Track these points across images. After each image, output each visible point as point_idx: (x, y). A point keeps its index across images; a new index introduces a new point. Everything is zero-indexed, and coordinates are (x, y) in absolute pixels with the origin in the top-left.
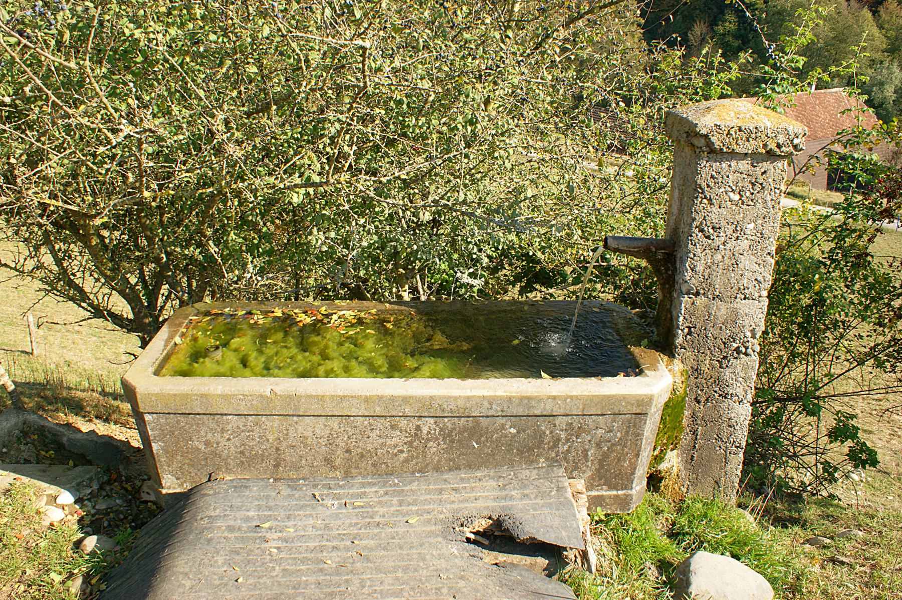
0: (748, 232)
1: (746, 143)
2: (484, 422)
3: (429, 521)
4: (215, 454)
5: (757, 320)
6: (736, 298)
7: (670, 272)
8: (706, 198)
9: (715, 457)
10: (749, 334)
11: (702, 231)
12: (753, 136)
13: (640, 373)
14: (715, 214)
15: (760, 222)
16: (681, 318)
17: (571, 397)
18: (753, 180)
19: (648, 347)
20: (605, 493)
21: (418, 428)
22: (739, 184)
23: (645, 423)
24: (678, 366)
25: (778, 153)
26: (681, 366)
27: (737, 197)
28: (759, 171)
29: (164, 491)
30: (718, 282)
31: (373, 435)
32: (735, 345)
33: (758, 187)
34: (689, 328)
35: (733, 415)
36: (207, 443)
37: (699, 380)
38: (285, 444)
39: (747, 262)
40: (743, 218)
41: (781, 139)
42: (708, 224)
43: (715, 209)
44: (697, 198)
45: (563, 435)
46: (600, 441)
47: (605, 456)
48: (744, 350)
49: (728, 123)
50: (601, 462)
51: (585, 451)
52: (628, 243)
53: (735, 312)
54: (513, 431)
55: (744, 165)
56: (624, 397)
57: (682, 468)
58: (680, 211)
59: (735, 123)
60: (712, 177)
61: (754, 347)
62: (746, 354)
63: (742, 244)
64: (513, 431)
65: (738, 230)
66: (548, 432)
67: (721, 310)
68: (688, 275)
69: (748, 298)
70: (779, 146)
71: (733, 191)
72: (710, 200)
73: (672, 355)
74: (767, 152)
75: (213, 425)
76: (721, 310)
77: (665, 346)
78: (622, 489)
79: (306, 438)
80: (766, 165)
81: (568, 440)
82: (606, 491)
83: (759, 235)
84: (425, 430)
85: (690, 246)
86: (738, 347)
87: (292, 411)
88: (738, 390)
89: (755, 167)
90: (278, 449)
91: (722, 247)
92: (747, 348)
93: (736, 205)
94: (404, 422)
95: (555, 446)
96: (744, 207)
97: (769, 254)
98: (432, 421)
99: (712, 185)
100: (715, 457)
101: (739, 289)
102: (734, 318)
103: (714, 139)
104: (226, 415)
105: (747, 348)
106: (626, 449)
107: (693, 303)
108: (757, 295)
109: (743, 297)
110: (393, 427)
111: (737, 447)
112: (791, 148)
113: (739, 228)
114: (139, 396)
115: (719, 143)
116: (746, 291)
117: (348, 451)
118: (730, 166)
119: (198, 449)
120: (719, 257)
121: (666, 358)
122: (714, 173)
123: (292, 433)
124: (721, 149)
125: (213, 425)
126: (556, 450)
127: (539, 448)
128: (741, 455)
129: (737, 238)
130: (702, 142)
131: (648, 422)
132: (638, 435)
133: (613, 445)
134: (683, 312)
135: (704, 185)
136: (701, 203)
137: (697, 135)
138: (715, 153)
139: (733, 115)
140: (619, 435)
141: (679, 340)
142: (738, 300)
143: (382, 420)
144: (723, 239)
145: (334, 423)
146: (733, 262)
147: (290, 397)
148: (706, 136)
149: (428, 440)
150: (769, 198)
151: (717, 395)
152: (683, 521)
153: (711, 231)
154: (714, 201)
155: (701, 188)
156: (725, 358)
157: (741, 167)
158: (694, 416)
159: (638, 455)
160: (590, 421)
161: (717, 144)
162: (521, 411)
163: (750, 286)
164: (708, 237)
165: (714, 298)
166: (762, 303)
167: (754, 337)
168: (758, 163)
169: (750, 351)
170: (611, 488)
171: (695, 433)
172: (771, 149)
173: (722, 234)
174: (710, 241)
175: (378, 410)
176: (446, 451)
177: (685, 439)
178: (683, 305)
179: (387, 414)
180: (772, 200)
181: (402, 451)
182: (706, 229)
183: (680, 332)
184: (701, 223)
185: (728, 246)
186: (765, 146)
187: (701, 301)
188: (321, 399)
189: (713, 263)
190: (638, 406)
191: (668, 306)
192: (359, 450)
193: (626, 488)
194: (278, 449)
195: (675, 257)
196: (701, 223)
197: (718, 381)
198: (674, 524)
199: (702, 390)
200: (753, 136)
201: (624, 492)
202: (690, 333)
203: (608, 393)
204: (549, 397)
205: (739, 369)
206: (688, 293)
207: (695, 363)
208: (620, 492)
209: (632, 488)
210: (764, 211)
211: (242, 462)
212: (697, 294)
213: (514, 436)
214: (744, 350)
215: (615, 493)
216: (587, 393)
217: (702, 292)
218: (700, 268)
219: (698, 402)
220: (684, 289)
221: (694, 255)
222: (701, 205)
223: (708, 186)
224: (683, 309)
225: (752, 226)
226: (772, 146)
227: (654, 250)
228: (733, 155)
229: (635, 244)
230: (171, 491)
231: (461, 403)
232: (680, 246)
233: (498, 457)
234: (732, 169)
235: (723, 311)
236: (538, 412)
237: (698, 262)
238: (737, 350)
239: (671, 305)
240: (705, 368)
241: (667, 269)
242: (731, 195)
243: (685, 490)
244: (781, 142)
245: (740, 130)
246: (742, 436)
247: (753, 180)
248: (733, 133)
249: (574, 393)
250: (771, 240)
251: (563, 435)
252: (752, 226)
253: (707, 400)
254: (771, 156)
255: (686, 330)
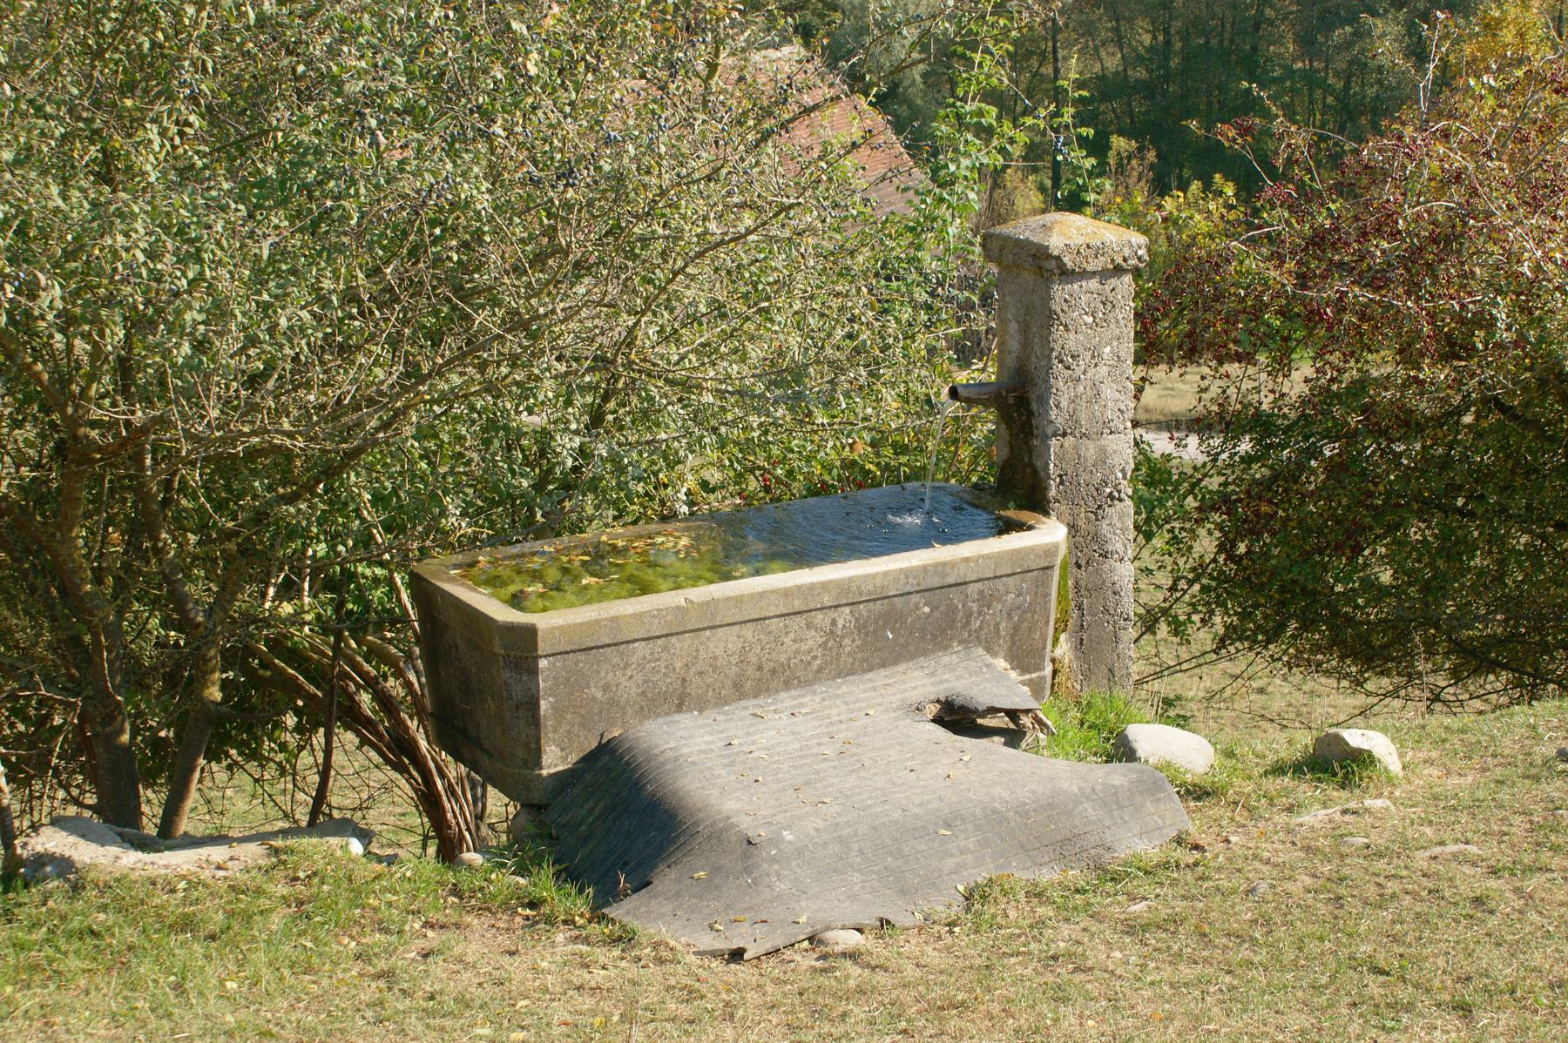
2: (898, 602)
3: (886, 710)
4: (612, 702)
10: (1120, 475)
11: (1061, 361)
14: (1072, 341)
21: (834, 623)
27: (1090, 320)
28: (1108, 288)
29: (544, 772)
30: (1083, 417)
31: (788, 641)
33: (1109, 306)
36: (606, 688)
38: (692, 672)
39: (1108, 391)
43: (1072, 336)
47: (1016, 628)
50: (1013, 636)
51: (997, 625)
52: (977, 389)
53: (1103, 450)
54: (927, 609)
55: (1093, 284)
58: (1026, 343)
59: (1080, 240)
62: (1120, 500)
64: (927, 609)
65: (1096, 355)
67: (1090, 450)
68: (1053, 413)
70: (1125, 260)
75: (616, 660)
76: (1090, 450)
79: (716, 658)
80: (1113, 282)
81: (980, 613)
84: (840, 623)
87: (709, 622)
90: (684, 680)
94: (820, 616)
95: (968, 623)
98: (847, 610)
102: (1103, 454)
103: (1066, 260)
104: (628, 642)
110: (809, 626)
114: (540, 639)
117: (760, 668)
119: (594, 699)
120: (1081, 388)
123: (702, 655)
125: (616, 660)
130: (1053, 264)
132: (1047, 595)
137: (1049, 257)
138: (1067, 275)
141: (1052, 493)
143: (798, 618)
145: (748, 631)
147: (707, 603)
148: (1058, 258)
149: (843, 637)
158: (1077, 586)
160: (999, 584)
161: (1070, 265)
162: (936, 582)
164: (1068, 368)
167: (1124, 478)
175: (798, 605)
176: (860, 649)
179: (800, 609)
181: (815, 658)
185: (1089, 375)
186: (1113, 261)
187: (1069, 441)
188: (738, 600)
192: (772, 664)
194: (684, 680)
197: (1096, 537)
202: (1062, 482)
206: (1055, 435)
211: (642, 708)
212: (1064, 435)
213: (928, 616)
218: (1064, 404)
220: (1049, 431)
222: (1058, 332)
225: (1108, 349)
226: (1119, 260)
228: (1085, 275)
229: (985, 390)
230: (553, 771)
231: (878, 582)
233: (912, 648)
235: (1092, 451)
236: (951, 581)
237: (1062, 398)
238: (1111, 496)
240: (1081, 523)
241: (1020, 415)
252: (1108, 349)
254: (1118, 270)
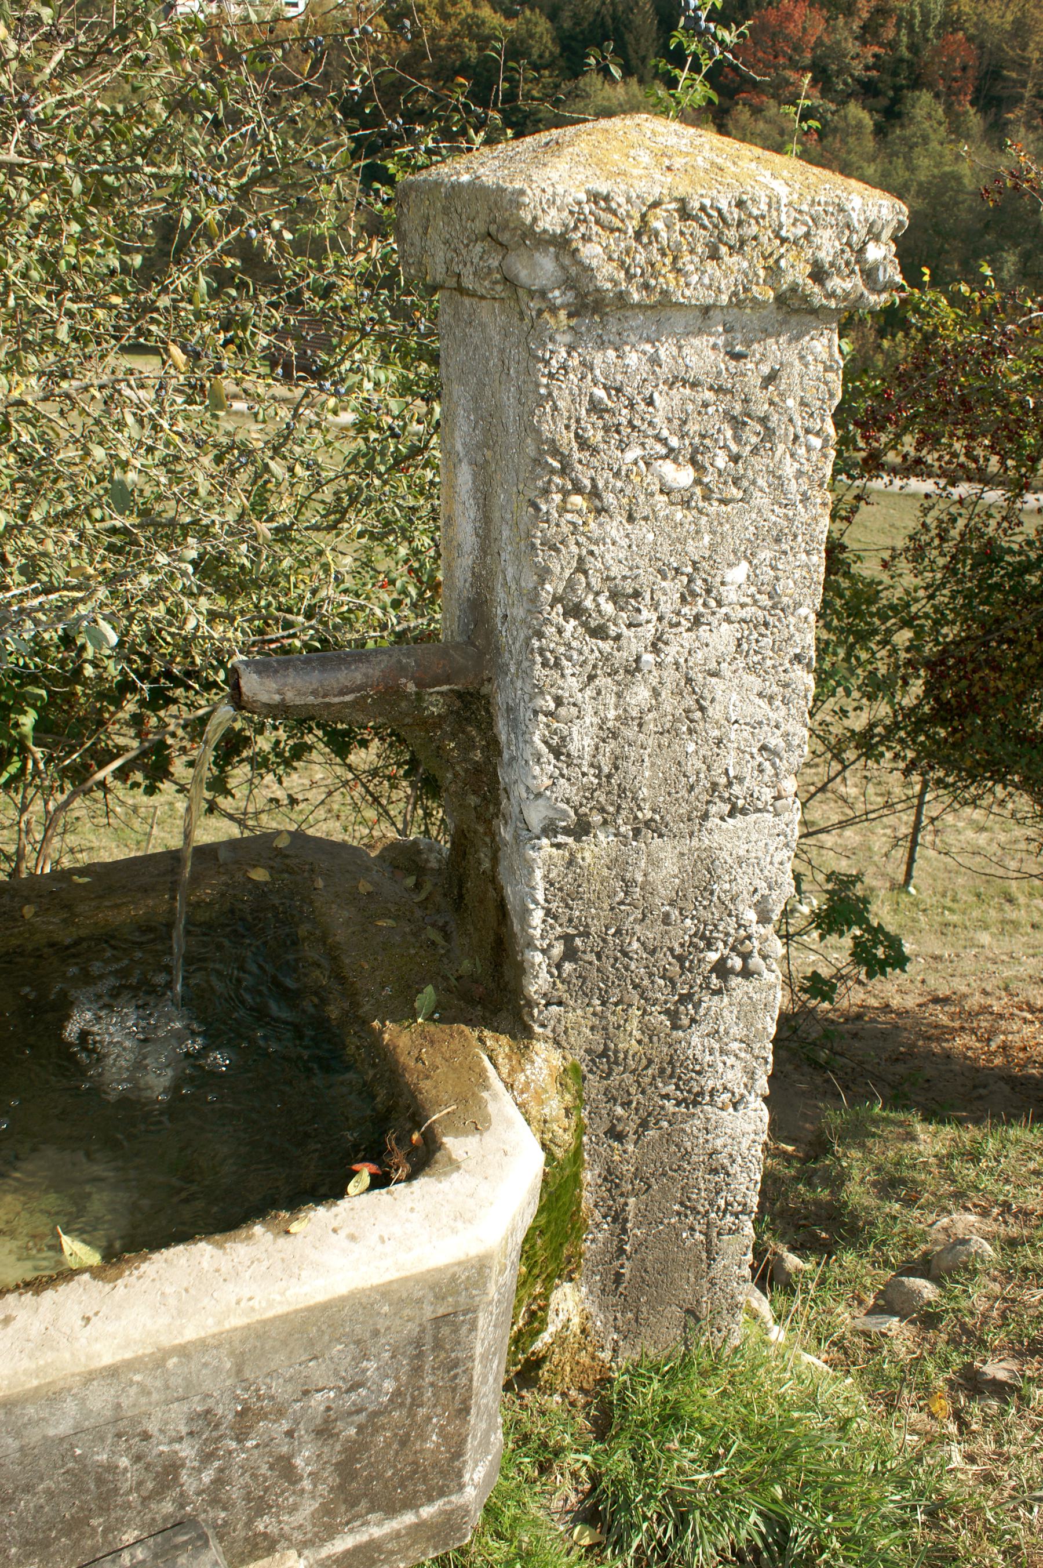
0: (730, 594)
1: (710, 266)
5: (771, 871)
6: (705, 816)
7: (478, 756)
8: (578, 489)
9: (681, 1256)
10: (751, 916)
11: (575, 611)
12: (731, 235)
13: (424, 1158)
14: (617, 546)
15: (765, 554)
16: (537, 916)
17: (183, 1351)
18: (738, 408)
19: (446, 1014)
20: (376, 1532)
22: (693, 427)
23: (473, 1328)
24: (545, 1060)
25: (818, 299)
26: (556, 1058)
28: (753, 371)
30: (646, 779)
32: (713, 957)
33: (752, 435)
34: (568, 939)
35: (719, 1143)
37: (615, 1080)
39: (733, 697)
40: (713, 547)
41: (827, 245)
42: (596, 582)
43: (615, 528)
44: (546, 492)
45: (187, 1451)
46: (326, 1421)
48: (737, 963)
49: (641, 187)
55: (702, 354)
56: (385, 1292)
57: (594, 1310)
60: (596, 407)
61: (768, 949)
62: (747, 973)
63: (713, 639)
65: (699, 588)
66: (124, 1462)
67: (665, 863)
68: (542, 773)
69: (744, 812)
71: (672, 454)
72: (595, 493)
73: (520, 1030)
74: (780, 299)
76: (665, 863)
77: (495, 999)
78: (430, 1500)
80: (775, 350)
81: (206, 1458)
82: (379, 1524)
83: (764, 600)
85: (538, 671)
86: (723, 960)
88: (730, 1075)
89: (737, 357)
91: (648, 658)
92: (746, 957)
93: (686, 504)
96: (713, 508)
97: (798, 658)
99: (595, 436)
100: (681, 1256)
101: (715, 785)
102: (705, 871)
103: (592, 253)
105: (746, 957)
106: (422, 1411)
107: (571, 862)
108: (768, 794)
109: (726, 808)
111: (736, 1215)
112: (858, 279)
113: (698, 586)
115: (609, 269)
116: (736, 789)
118: (655, 361)
120: (640, 695)
121: (502, 1045)
122: (600, 393)
124: (621, 297)
126: (175, 1493)
127: (104, 1510)
128: (749, 1229)
129: (697, 621)
131: (481, 1323)
133: (376, 1414)
134: (540, 897)
135: (566, 439)
136: (563, 510)
138: (593, 308)
139: (645, 159)
140: (389, 1385)
141: (539, 983)
142: (713, 822)
144: (649, 632)
146: (690, 702)
150: (789, 469)
151: (670, 1105)
152: (620, 1462)
153: (608, 608)
154: (609, 498)
155: (556, 452)
156: (684, 999)
157: (692, 360)
158: (610, 1177)
159: (464, 1411)
161: (606, 275)
163: (747, 772)
164: (598, 632)
165: (637, 832)
166: (786, 817)
168: (748, 344)
169: (756, 961)
170: (392, 1510)
171: (618, 1218)
172: (794, 289)
173: (646, 614)
174: (606, 646)
177: (594, 1242)
178: (539, 874)
180: (799, 474)
182: (588, 603)
183: (538, 957)
184: (571, 585)
185: (671, 653)
186: (774, 271)
187: (597, 848)
189: (624, 720)
190: (440, 1298)
191: (486, 865)
193: (442, 1494)
195: (487, 702)
196: (571, 585)
197: (673, 1068)
198: (595, 1479)
199: (626, 1105)
200: (731, 235)
201: (439, 1504)
202: (571, 954)
203: (321, 1298)
204: (90, 1377)
205: (729, 1017)
206: (550, 830)
207: (598, 1037)
208: (427, 1512)
209: (461, 1487)
210: (776, 517)
212: (581, 829)
214: (737, 963)
215: (409, 1518)
216: (237, 1321)
217: (596, 818)
219: (620, 1137)
221: (559, 701)
223: (583, 444)
224: (540, 885)
225: (739, 573)
227: (411, 688)
232: (504, 670)
234: (664, 372)
235: (670, 866)
238: (721, 969)
239: (495, 860)
240: (630, 1042)
241: (468, 746)
242: (667, 468)
243: (606, 1355)
244: (825, 256)
245: (684, 213)
246: (746, 1186)
247: (738, 408)
248: (659, 225)
249: (190, 1334)
250: (803, 611)
251: (187, 1451)
252: (739, 573)
253: (644, 1125)
255: (558, 949)
